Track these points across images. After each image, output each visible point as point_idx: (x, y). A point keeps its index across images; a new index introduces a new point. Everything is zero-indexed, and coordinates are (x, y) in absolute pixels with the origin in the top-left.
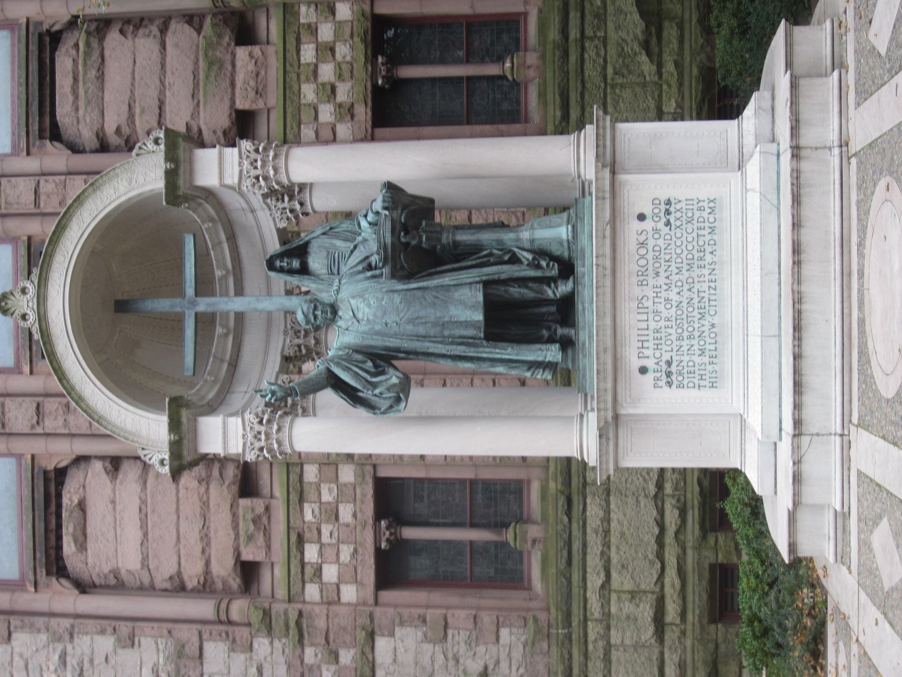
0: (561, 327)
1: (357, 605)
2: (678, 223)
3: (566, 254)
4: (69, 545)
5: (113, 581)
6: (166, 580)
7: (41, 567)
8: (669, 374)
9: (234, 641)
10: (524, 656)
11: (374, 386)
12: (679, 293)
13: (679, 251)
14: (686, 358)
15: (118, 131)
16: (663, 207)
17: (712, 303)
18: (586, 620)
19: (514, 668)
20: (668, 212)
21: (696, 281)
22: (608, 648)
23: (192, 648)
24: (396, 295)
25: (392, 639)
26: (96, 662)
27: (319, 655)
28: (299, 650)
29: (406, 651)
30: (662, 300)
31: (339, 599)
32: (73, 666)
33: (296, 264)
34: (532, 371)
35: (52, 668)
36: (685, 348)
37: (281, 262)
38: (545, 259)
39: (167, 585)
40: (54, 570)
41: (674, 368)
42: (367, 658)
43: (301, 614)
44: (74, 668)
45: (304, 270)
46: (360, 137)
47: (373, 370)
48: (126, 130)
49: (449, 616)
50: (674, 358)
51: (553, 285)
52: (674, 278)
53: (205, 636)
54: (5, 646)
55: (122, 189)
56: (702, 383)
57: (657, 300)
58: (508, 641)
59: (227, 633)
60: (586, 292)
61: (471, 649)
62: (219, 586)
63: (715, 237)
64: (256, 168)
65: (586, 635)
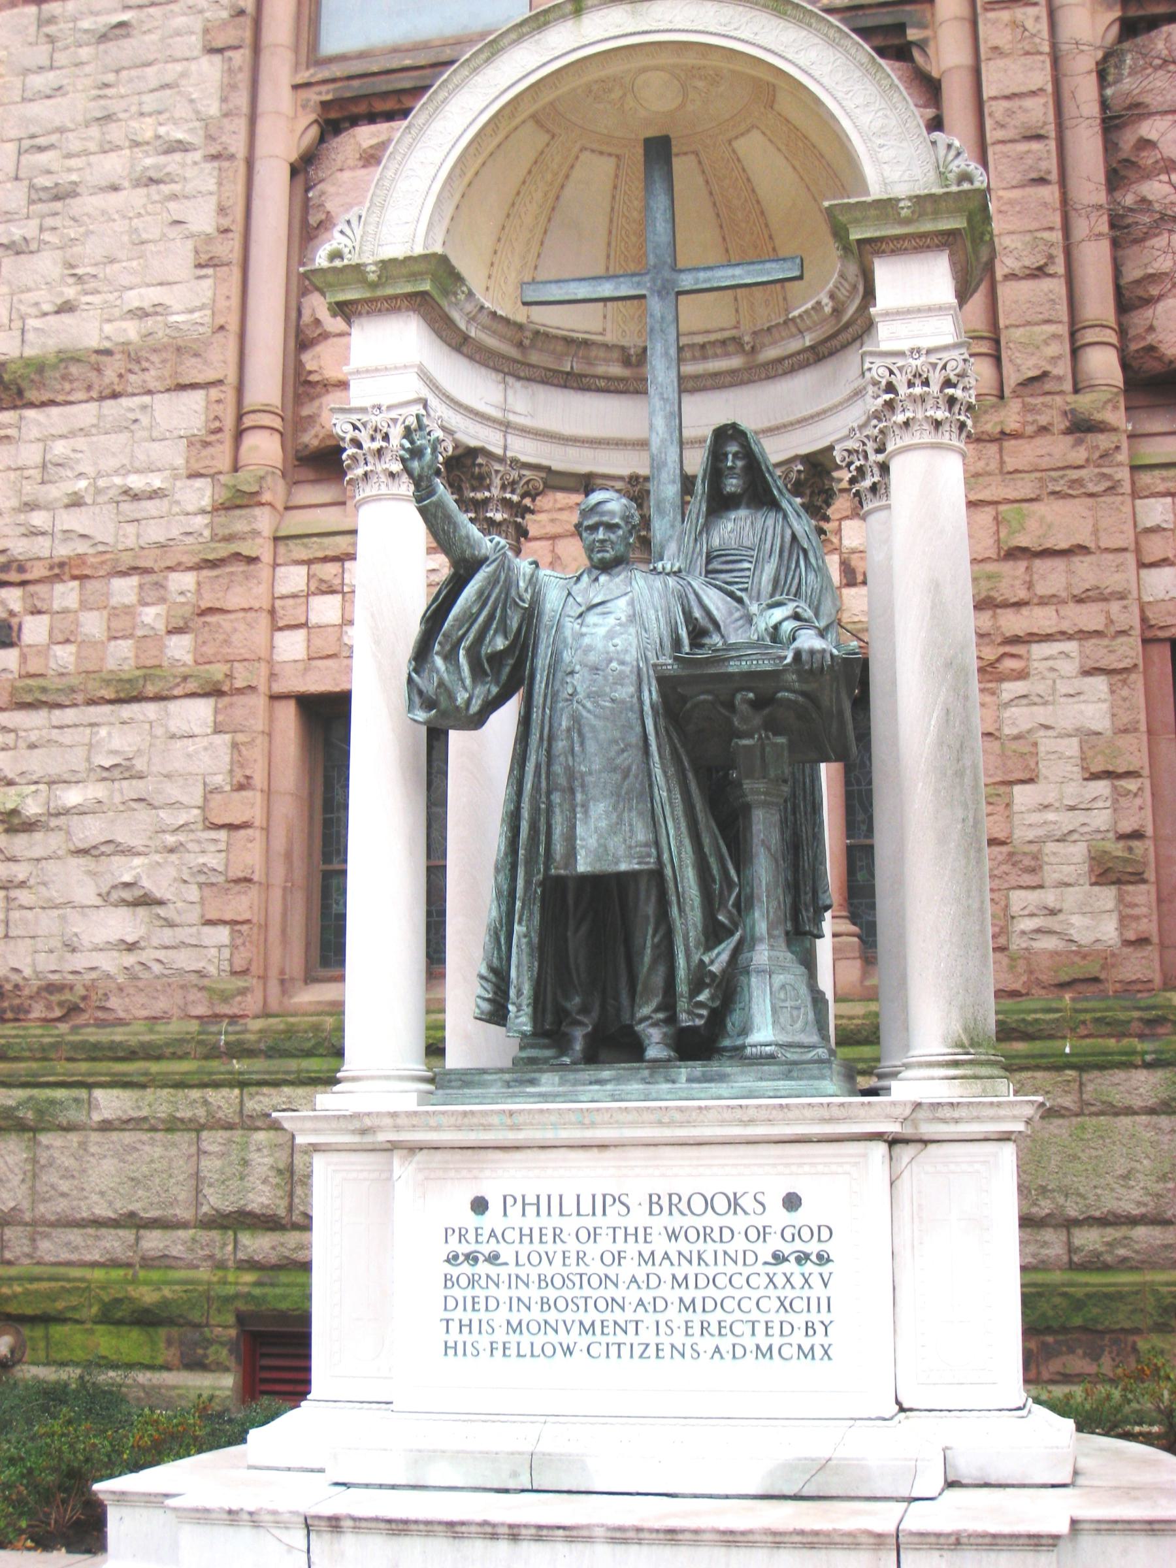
0: (586, 1036)
1: (270, 662)
2: (780, 1280)
3: (727, 1043)
4: (373, 135)
5: (313, 220)
6: (313, 313)
7: (335, 90)
8: (471, 1258)
9: (206, 444)
10: (181, 972)
11: (450, 657)
12: (634, 1280)
13: (722, 1281)
14: (503, 1293)
15: (1146, 144)
16: (813, 1248)
17: (613, 1350)
18: (242, 1085)
19: (161, 954)
20: (803, 1258)
21: (658, 1316)
22: (192, 1125)
23: (194, 371)
24: (632, 689)
25: (209, 731)
26: (172, 205)
27: (182, 599)
28: (190, 560)
29: (189, 756)
30: (620, 1245)
31: (280, 629)
32: (165, 166)
33: (732, 485)
34: (491, 976)
35: (162, 130)
36: (523, 1292)
37: (735, 455)
38: (713, 998)
39: (306, 318)
40: (333, 115)
41: (483, 1268)
42: (178, 685)
43: (252, 560)
44: (158, 167)
45: (720, 504)
46: (1150, 614)
47: (486, 650)
48: (1148, 159)
49: (250, 831)
50: (504, 1271)
51: (661, 1016)
52: (665, 1271)
53: (214, 393)
54: (199, 46)
55: (865, 119)
56: (454, 1326)
57: (620, 1234)
58: (206, 942)
59: (219, 430)
60: (635, 1087)
61: (193, 875)
62: (305, 412)
63: (750, 1357)
64: (910, 384)
65: (216, 1085)
